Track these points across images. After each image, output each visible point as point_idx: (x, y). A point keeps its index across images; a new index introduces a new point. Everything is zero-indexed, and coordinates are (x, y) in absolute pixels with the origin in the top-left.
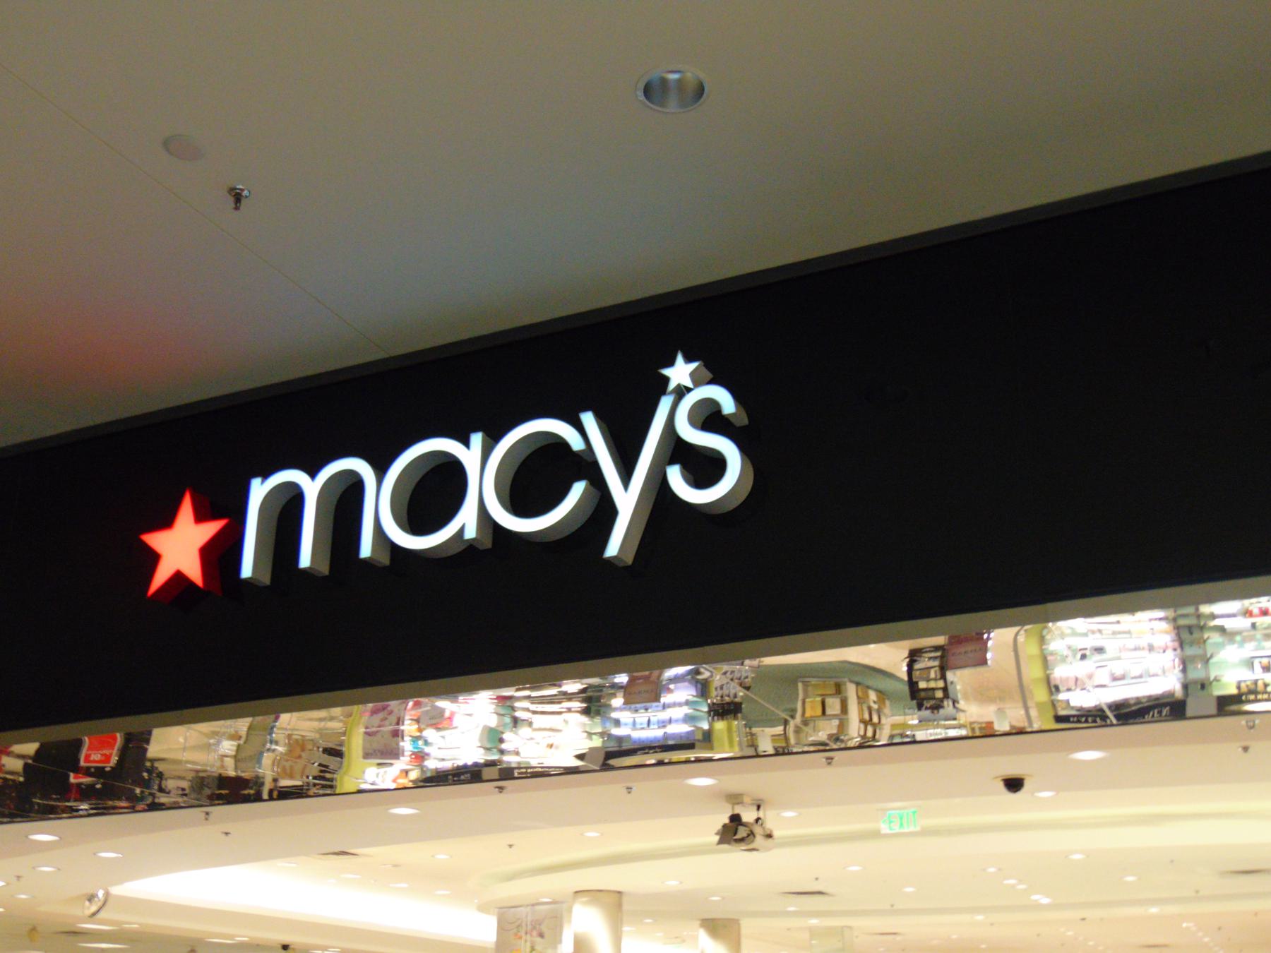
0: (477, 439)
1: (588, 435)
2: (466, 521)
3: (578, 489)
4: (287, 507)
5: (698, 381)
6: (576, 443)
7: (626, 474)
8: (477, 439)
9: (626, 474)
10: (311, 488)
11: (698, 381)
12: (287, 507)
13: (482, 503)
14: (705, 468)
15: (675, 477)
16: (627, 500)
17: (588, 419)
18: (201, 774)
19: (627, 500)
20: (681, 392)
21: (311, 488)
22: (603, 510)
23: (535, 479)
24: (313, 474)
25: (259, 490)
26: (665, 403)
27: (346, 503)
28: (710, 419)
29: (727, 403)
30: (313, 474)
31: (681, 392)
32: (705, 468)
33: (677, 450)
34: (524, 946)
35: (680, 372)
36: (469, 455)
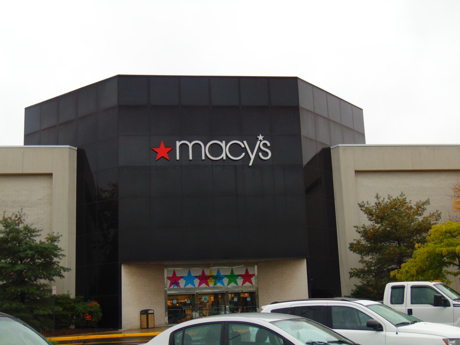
0: (224, 142)
1: (245, 144)
2: (223, 156)
3: (244, 154)
4: (184, 147)
5: (264, 139)
6: (243, 146)
7: (252, 154)
8: (224, 142)
9: (252, 154)
10: (190, 145)
11: (264, 139)
12: (184, 147)
13: (226, 153)
14: (266, 154)
15: (260, 154)
16: (252, 157)
17: (245, 142)
18: (453, 324)
19: (252, 157)
20: (261, 141)
21: (190, 145)
22: (247, 157)
23: (235, 150)
24: (190, 143)
25: (178, 144)
26: (258, 142)
27: (197, 148)
28: (265, 145)
29: (269, 144)
30: (190, 143)
31: (261, 141)
32: (266, 154)
33: (259, 150)
34: (3, 262)
35: (261, 137)
36: (223, 144)
